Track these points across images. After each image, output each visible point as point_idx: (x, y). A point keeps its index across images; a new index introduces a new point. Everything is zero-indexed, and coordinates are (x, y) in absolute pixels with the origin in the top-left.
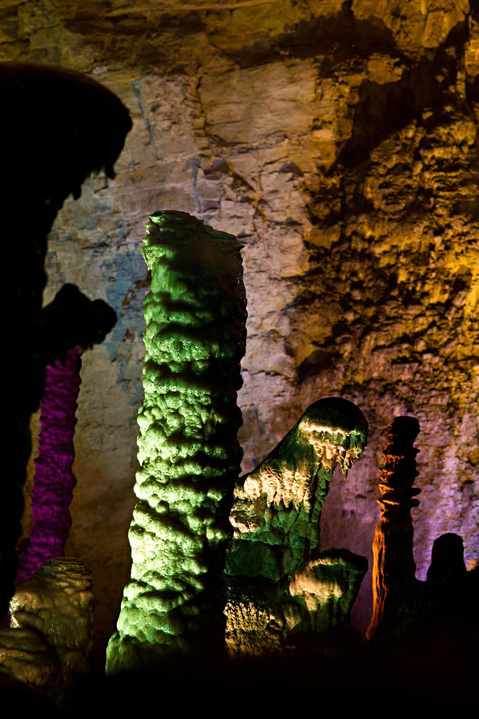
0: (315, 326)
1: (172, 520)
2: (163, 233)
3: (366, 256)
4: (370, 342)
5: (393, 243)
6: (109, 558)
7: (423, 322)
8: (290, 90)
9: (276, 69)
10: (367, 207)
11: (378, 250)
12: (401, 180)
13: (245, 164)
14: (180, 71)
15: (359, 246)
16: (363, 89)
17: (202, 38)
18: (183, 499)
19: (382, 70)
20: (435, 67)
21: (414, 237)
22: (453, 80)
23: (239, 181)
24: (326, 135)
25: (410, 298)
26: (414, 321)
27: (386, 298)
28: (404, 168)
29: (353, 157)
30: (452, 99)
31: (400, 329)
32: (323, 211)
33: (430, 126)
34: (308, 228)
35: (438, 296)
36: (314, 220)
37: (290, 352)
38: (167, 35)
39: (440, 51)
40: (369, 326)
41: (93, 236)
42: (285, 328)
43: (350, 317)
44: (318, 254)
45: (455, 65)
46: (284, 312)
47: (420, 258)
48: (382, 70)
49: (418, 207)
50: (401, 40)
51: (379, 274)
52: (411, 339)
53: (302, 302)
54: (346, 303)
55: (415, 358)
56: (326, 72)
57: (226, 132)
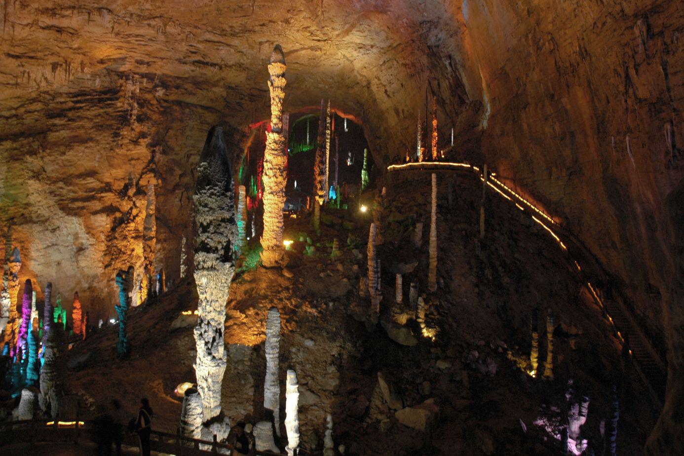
0: (108, 259)
1: (33, 357)
2: (92, 396)
3: (116, 246)
4: (117, 261)
5: (121, 244)
6: (405, 65)
7: (127, 257)
8: (102, 219)
9: (99, 215)
10: (116, 238)
11: (118, 245)
12: (122, 234)
13: (94, 232)
14: (81, 216)
15: (115, 245)
16: (115, 218)
17: (85, 210)
18: (33, 355)
19: (118, 215)
20: (127, 214)
21: (125, 243)
22: (130, 216)
23: (93, 235)
24: (108, 226)
25: (124, 253)
26: (125, 257)
27: (120, 253)
28: (122, 231)
29: (113, 229)
30: (130, 219)
31: (122, 259)
32: (108, 239)
33: (127, 224)
34: (106, 242)
35: (129, 252)
36: (107, 241)
37: (103, 263)
38: (79, 210)
39: (128, 211)
40: (117, 258)
41: (67, 245)
42: (102, 259)
43: (114, 257)
44: (108, 247)
45: (131, 213)
46: (102, 256)
47: (126, 246)
48: (118, 215)
49: (125, 238)
50: (121, 210)
51: (118, 249)
52: (124, 260)
53: (105, 255)
54: (113, 255)
55: (125, 263)
56: (108, 215)
57: (90, 226)
